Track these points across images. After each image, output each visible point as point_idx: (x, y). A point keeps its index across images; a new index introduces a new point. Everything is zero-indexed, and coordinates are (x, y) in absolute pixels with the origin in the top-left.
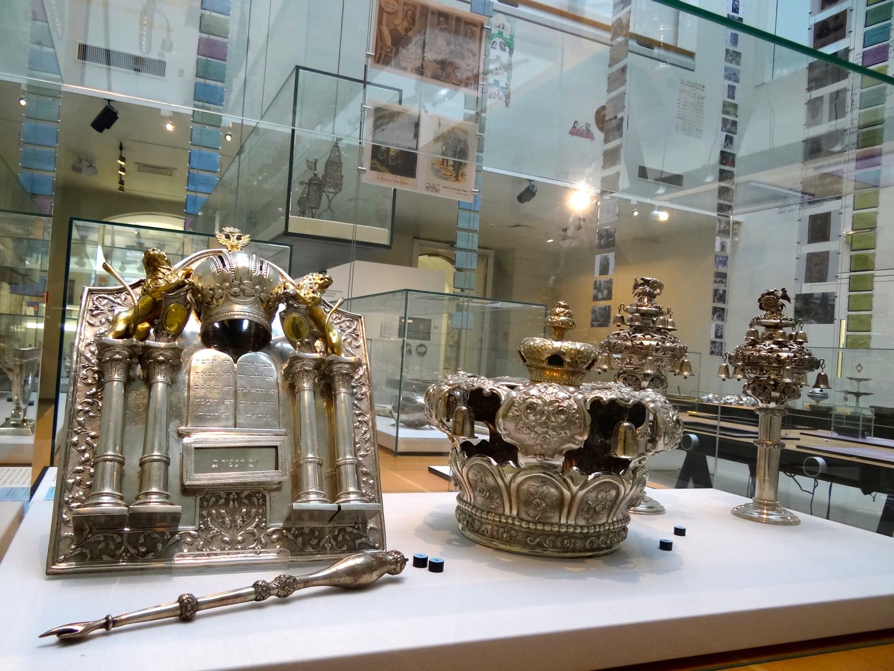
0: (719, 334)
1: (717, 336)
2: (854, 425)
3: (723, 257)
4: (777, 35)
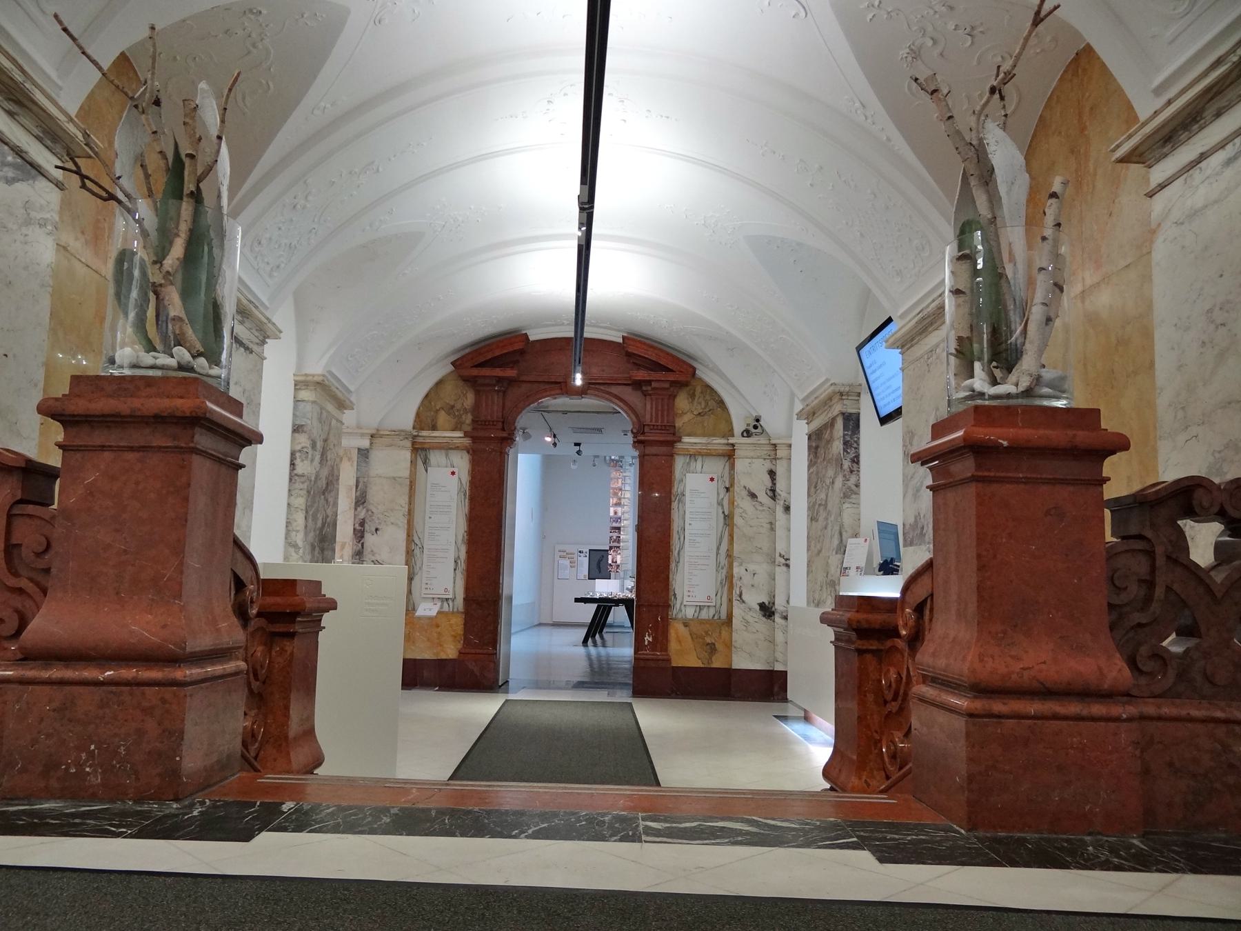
1: (613, 562)
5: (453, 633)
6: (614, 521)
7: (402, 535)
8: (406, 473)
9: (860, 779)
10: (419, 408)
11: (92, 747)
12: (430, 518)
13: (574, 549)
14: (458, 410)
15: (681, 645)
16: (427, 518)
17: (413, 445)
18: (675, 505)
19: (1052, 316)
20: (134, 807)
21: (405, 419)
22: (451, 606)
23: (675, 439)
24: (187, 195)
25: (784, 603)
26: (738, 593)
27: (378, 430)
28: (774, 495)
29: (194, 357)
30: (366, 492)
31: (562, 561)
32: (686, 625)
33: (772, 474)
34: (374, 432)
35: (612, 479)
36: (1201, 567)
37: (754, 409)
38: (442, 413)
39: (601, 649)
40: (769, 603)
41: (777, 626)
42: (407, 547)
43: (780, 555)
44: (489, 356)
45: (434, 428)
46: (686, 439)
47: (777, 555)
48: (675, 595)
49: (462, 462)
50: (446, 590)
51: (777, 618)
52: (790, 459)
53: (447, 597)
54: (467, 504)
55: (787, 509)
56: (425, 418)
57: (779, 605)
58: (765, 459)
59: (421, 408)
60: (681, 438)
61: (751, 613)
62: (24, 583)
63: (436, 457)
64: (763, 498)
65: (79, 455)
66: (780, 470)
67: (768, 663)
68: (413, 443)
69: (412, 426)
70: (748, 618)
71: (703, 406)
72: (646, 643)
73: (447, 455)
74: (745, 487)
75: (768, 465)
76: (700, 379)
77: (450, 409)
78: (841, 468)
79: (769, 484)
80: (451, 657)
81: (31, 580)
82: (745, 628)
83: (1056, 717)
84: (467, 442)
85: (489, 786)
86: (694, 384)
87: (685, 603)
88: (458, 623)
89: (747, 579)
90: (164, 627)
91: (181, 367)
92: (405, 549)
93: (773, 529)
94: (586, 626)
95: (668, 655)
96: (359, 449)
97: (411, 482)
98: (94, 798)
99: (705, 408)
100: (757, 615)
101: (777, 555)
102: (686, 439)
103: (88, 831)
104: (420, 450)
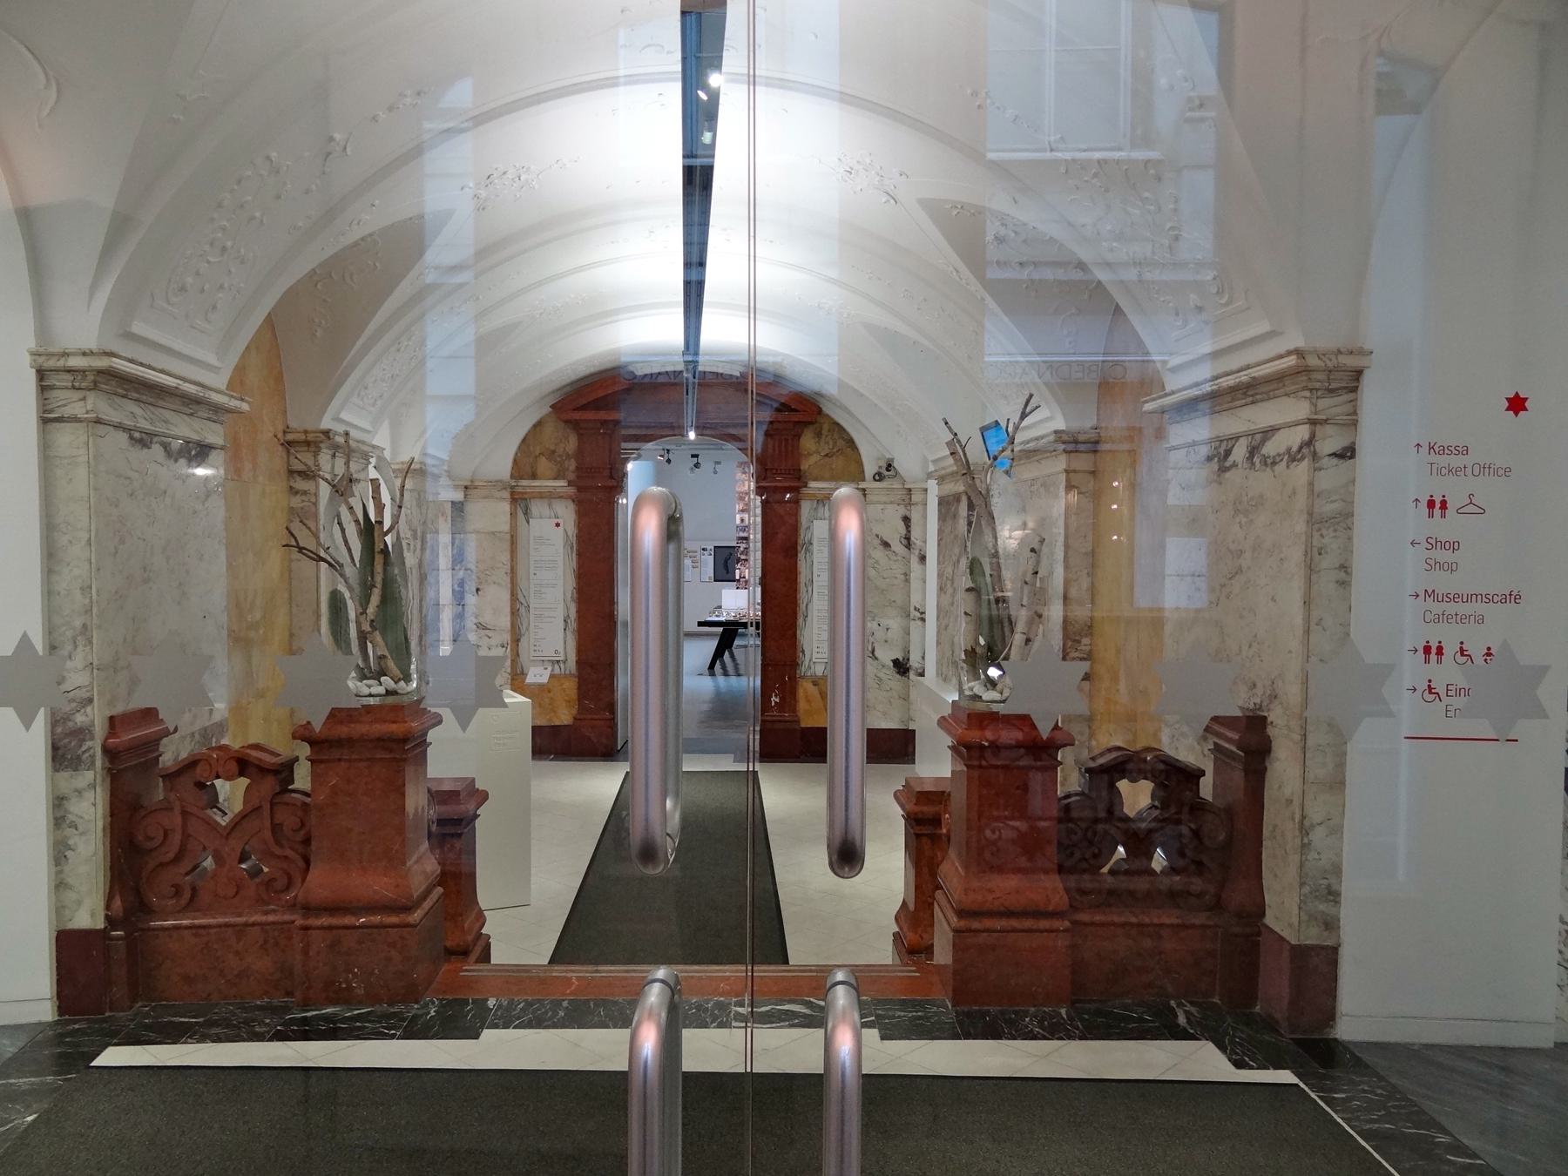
5: (566, 698)
7: (505, 596)
8: (506, 528)
9: (916, 933)
10: (516, 454)
11: (356, 970)
12: (535, 574)
14: (560, 456)
15: (811, 706)
16: (531, 574)
17: (511, 495)
18: (801, 555)
19: (1032, 636)
21: (501, 466)
22: (563, 670)
23: (802, 484)
24: (378, 552)
25: (919, 658)
26: (870, 649)
27: (472, 481)
28: (909, 543)
29: (396, 683)
30: (463, 550)
32: (815, 684)
33: (907, 520)
34: (469, 484)
35: (737, 481)
37: (888, 451)
38: (543, 459)
39: (733, 680)
40: (904, 659)
41: (911, 684)
42: (512, 608)
43: (915, 608)
44: (591, 398)
45: (534, 476)
46: (813, 484)
47: (912, 609)
48: (803, 652)
49: (567, 513)
50: (556, 652)
51: (912, 675)
52: (926, 504)
53: (558, 659)
54: (574, 559)
55: (923, 558)
56: (524, 467)
57: (914, 661)
58: (899, 505)
59: (519, 455)
60: (807, 483)
61: (884, 670)
62: (289, 852)
63: (537, 508)
64: (898, 547)
65: (322, 766)
66: (915, 517)
67: (903, 722)
68: (512, 494)
69: (509, 475)
70: (881, 675)
71: (831, 447)
72: (773, 704)
73: (550, 505)
74: (877, 536)
75: (902, 511)
76: (828, 416)
77: (551, 455)
78: (965, 550)
79: (904, 532)
80: (566, 723)
81: (291, 848)
82: (878, 686)
83: (1014, 930)
84: (572, 490)
85: (627, 971)
86: (822, 421)
87: (814, 660)
88: (571, 686)
89: (880, 634)
90: (397, 886)
91: (389, 693)
92: (509, 609)
93: (907, 581)
94: (716, 635)
95: (797, 716)
96: (452, 502)
97: (512, 536)
98: (361, 1004)
99: (833, 449)
100: (889, 673)
101: (912, 609)
102: (813, 484)
103: (369, 1034)
104: (519, 501)
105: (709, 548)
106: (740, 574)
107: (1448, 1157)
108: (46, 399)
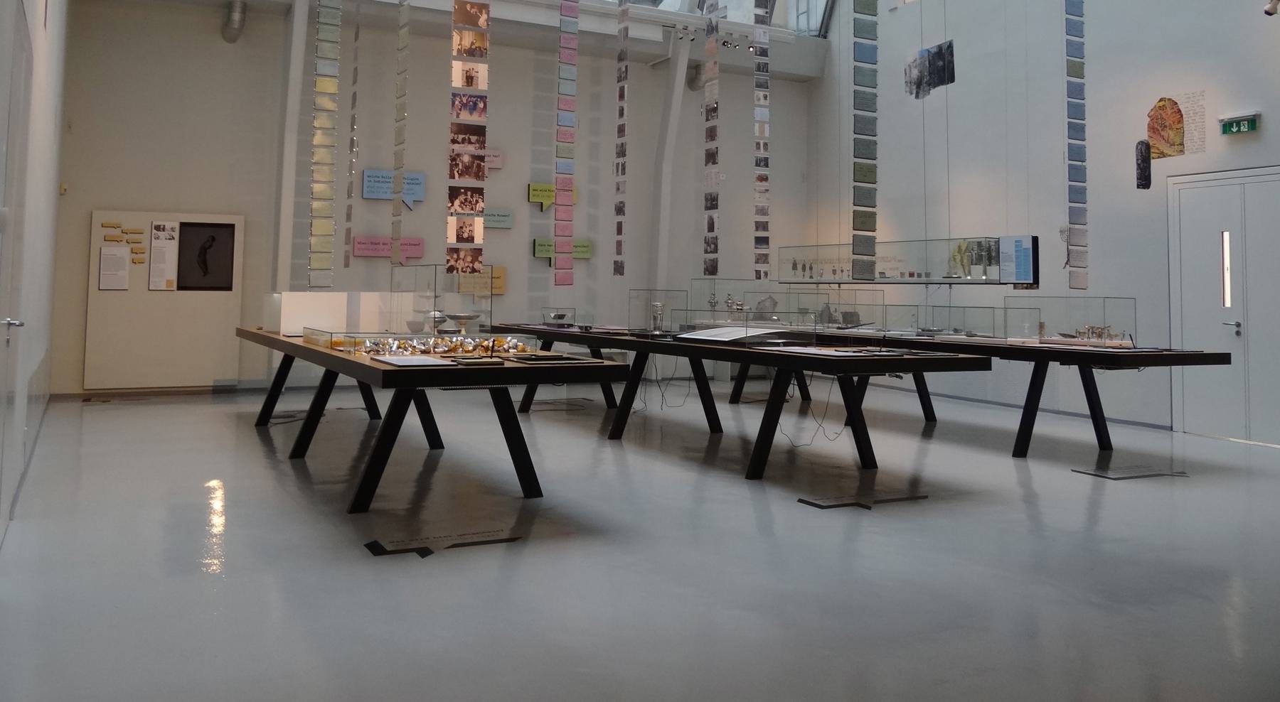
0: (466, 235)
1: (460, 239)
2: (302, 251)
3: (470, 96)
4: (1023, 403)
6: (464, 106)
13: (141, 221)
20: (485, 120)
31: (109, 250)
36: (602, 386)
105: (168, 225)
106: (460, 230)
107: (218, 522)
108: (713, 305)
